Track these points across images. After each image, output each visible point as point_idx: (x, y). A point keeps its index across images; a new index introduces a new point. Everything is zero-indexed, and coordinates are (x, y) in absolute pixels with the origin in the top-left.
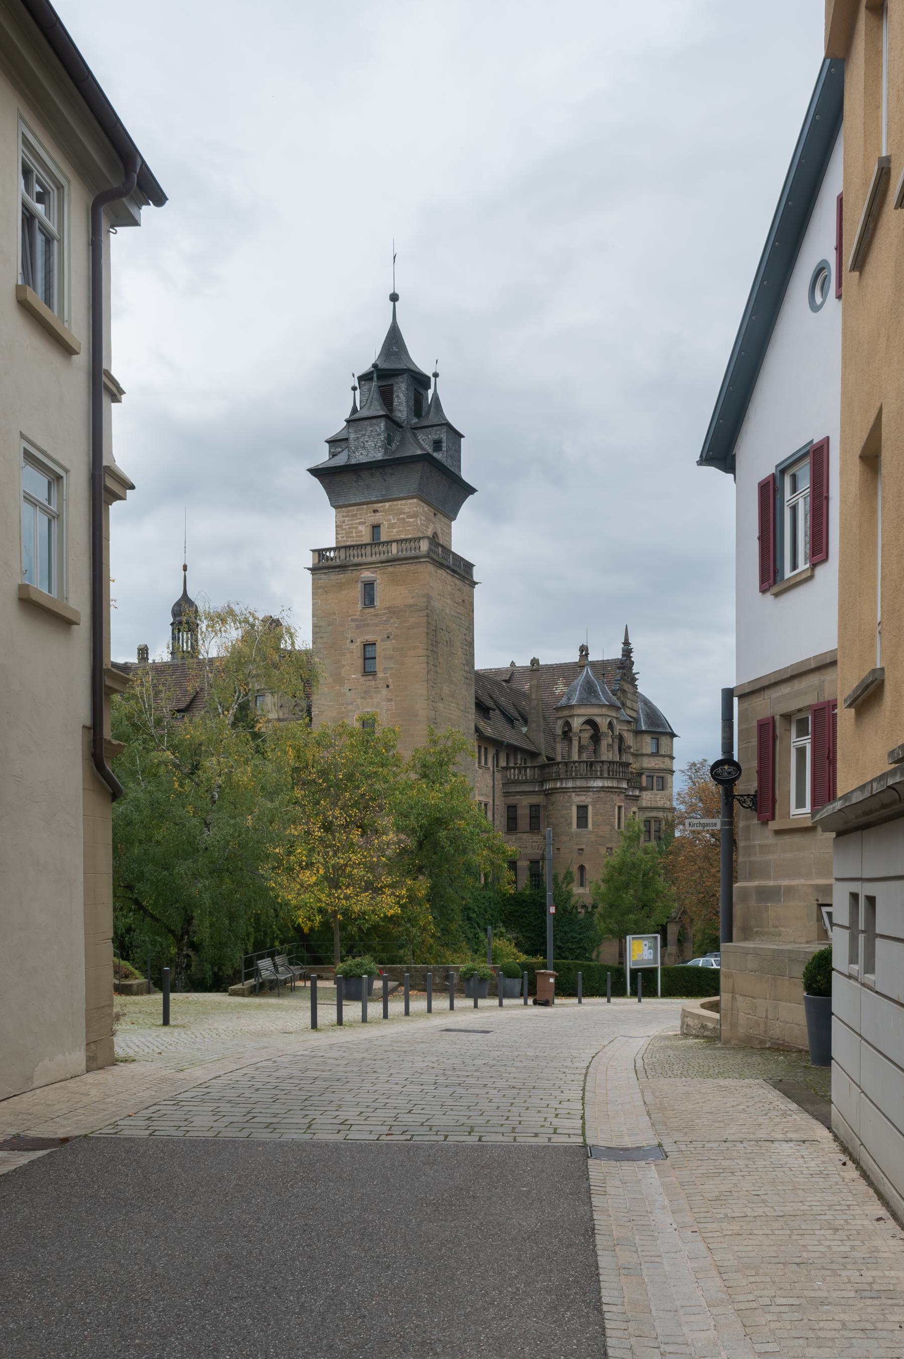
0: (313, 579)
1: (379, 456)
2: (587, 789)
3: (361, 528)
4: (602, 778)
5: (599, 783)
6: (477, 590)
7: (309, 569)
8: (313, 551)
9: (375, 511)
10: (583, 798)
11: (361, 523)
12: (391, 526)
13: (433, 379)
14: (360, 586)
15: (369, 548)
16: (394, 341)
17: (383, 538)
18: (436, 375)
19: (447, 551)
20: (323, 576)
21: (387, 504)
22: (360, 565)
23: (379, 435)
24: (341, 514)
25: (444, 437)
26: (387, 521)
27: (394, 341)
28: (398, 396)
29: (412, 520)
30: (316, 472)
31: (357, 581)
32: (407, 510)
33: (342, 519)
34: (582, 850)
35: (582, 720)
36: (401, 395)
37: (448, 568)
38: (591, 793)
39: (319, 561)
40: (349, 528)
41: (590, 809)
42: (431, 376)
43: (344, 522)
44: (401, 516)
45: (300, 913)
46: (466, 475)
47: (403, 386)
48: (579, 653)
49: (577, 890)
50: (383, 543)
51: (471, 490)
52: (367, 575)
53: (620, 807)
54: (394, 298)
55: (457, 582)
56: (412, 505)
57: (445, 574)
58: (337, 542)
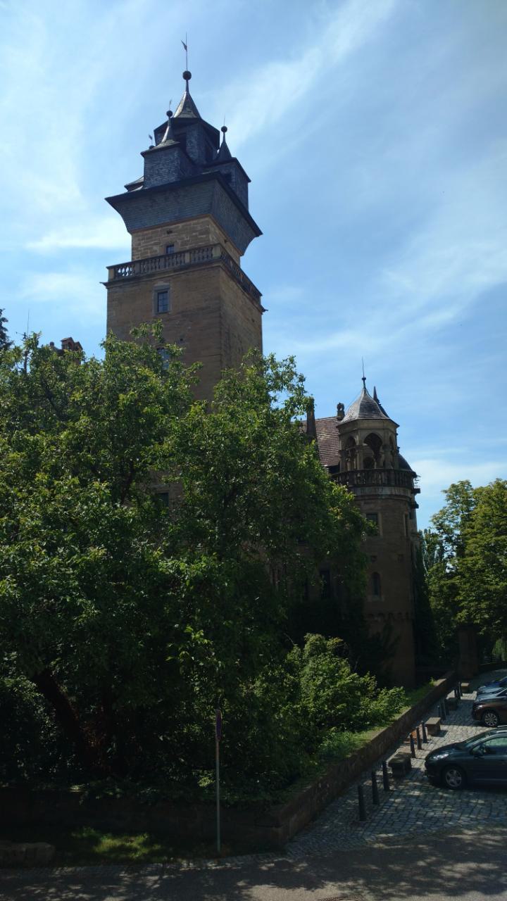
0: (109, 294)
1: (173, 179)
2: (375, 497)
3: (155, 248)
4: (389, 485)
5: (387, 491)
6: (264, 315)
7: (105, 284)
8: (109, 268)
9: (169, 232)
10: (372, 506)
11: (155, 244)
12: (184, 243)
13: (222, 134)
14: (153, 295)
15: (162, 260)
16: (189, 104)
17: (176, 249)
18: (224, 129)
19: (237, 266)
20: (118, 289)
21: (180, 225)
22: (153, 275)
23: (172, 162)
24: (137, 238)
25: (233, 171)
26: (179, 239)
27: (189, 104)
28: (191, 142)
29: (204, 236)
30: (114, 202)
31: (150, 291)
32: (199, 228)
33: (138, 242)
34: (375, 557)
35: (365, 434)
36: (193, 140)
37: (239, 282)
38: (379, 501)
39: (115, 278)
40: (144, 249)
41: (380, 515)
42: (220, 129)
43: (139, 244)
44: (194, 234)
45: (328, 741)
46: (254, 211)
47: (195, 133)
48: (337, 410)
49: (370, 598)
50: (177, 253)
51: (258, 233)
52: (160, 284)
53: (406, 516)
54: (187, 76)
55: (247, 301)
56: (208, 223)
57: (236, 287)
58: (132, 259)
